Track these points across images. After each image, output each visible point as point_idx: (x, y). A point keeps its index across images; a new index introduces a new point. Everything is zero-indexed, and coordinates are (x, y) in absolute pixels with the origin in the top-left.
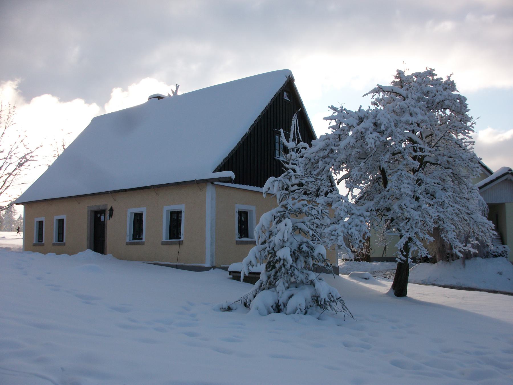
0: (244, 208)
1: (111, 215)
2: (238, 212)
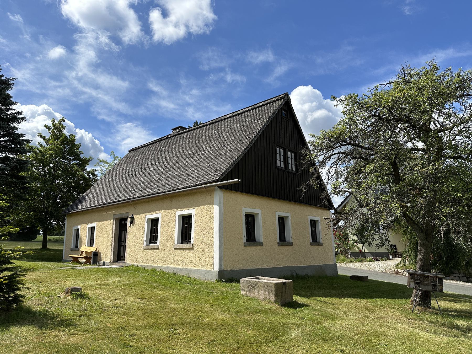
0: (283, 214)
1: (132, 222)
2: (245, 215)
